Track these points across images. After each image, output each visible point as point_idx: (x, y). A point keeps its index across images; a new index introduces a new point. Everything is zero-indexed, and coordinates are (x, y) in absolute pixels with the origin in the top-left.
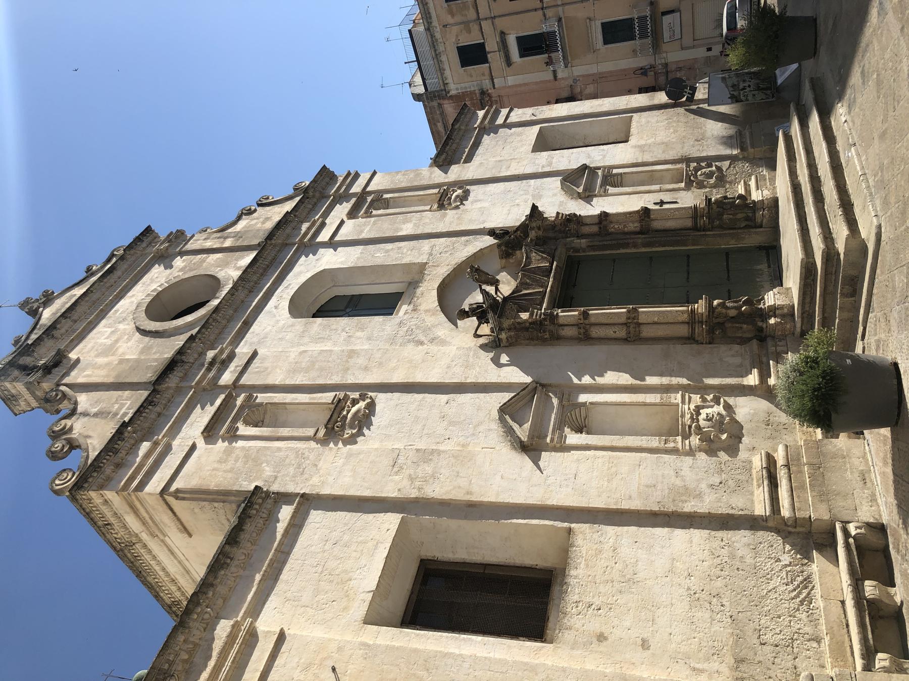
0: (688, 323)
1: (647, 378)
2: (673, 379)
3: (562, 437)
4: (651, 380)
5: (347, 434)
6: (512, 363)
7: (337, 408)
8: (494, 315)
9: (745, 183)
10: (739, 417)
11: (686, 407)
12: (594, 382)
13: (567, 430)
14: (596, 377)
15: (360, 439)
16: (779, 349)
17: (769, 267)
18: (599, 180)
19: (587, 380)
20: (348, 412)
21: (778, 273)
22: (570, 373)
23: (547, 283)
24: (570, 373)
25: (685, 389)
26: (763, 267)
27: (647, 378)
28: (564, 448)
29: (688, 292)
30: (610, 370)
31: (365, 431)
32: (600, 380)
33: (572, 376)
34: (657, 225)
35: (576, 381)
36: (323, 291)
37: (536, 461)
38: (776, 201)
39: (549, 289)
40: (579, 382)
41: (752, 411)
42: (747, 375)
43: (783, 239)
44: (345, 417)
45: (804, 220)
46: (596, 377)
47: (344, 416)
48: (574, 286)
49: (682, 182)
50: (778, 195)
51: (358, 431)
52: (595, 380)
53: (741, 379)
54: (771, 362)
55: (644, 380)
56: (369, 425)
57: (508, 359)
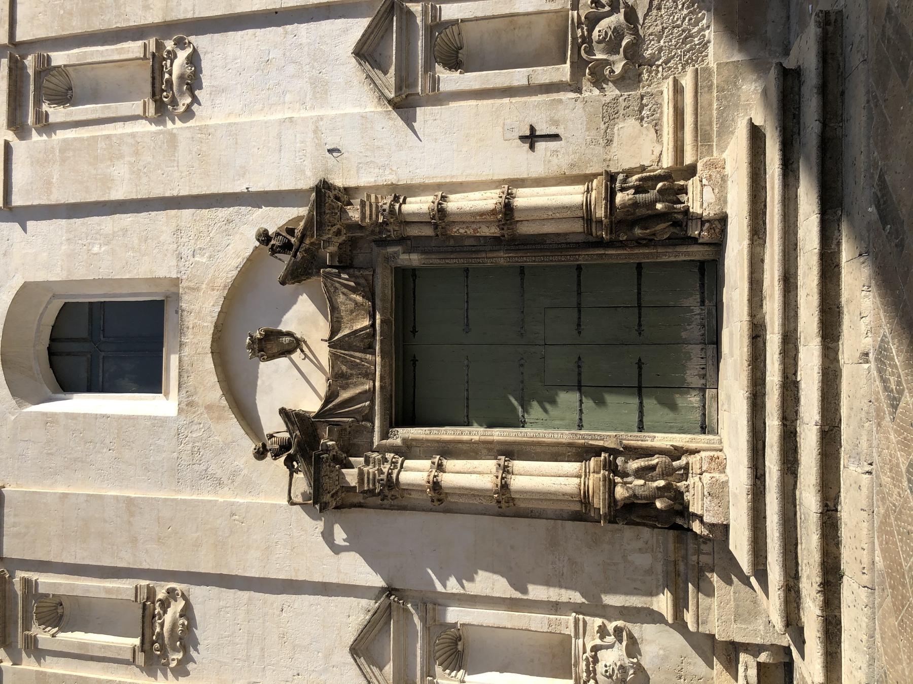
0: (583, 218)
1: (531, 587)
2: (563, 591)
3: (435, 82)
4: (537, 592)
5: (173, 660)
6: (354, 545)
7: (145, 620)
8: (307, 465)
9: (676, 82)
10: (646, 662)
11: (580, 641)
12: (462, 591)
13: (439, 68)
14: (464, 581)
15: (190, 666)
16: (704, 559)
17: (703, 302)
18: (420, 42)
19: (453, 586)
20: (162, 625)
21: (715, 322)
22: (430, 571)
23: (373, 367)
24: (430, 571)
25: (578, 609)
26: (692, 301)
27: (531, 587)
28: (438, 98)
29: (579, 358)
30: (482, 569)
31: (193, 653)
32: (472, 588)
33: (434, 577)
34: (525, 229)
35: (439, 588)
36: (42, 309)
37: (409, 121)
38: (723, 220)
39: (377, 384)
40: (443, 590)
41: (661, 652)
42: (657, 594)
43: (728, 322)
44: (161, 635)
45: (760, 446)
46: (464, 581)
47: (158, 633)
48: (414, 332)
49: (565, 63)
50: (729, 212)
51: (184, 655)
52: (463, 587)
53: (649, 599)
54: (690, 585)
55: (525, 591)
56: (195, 644)
57: (345, 536)
